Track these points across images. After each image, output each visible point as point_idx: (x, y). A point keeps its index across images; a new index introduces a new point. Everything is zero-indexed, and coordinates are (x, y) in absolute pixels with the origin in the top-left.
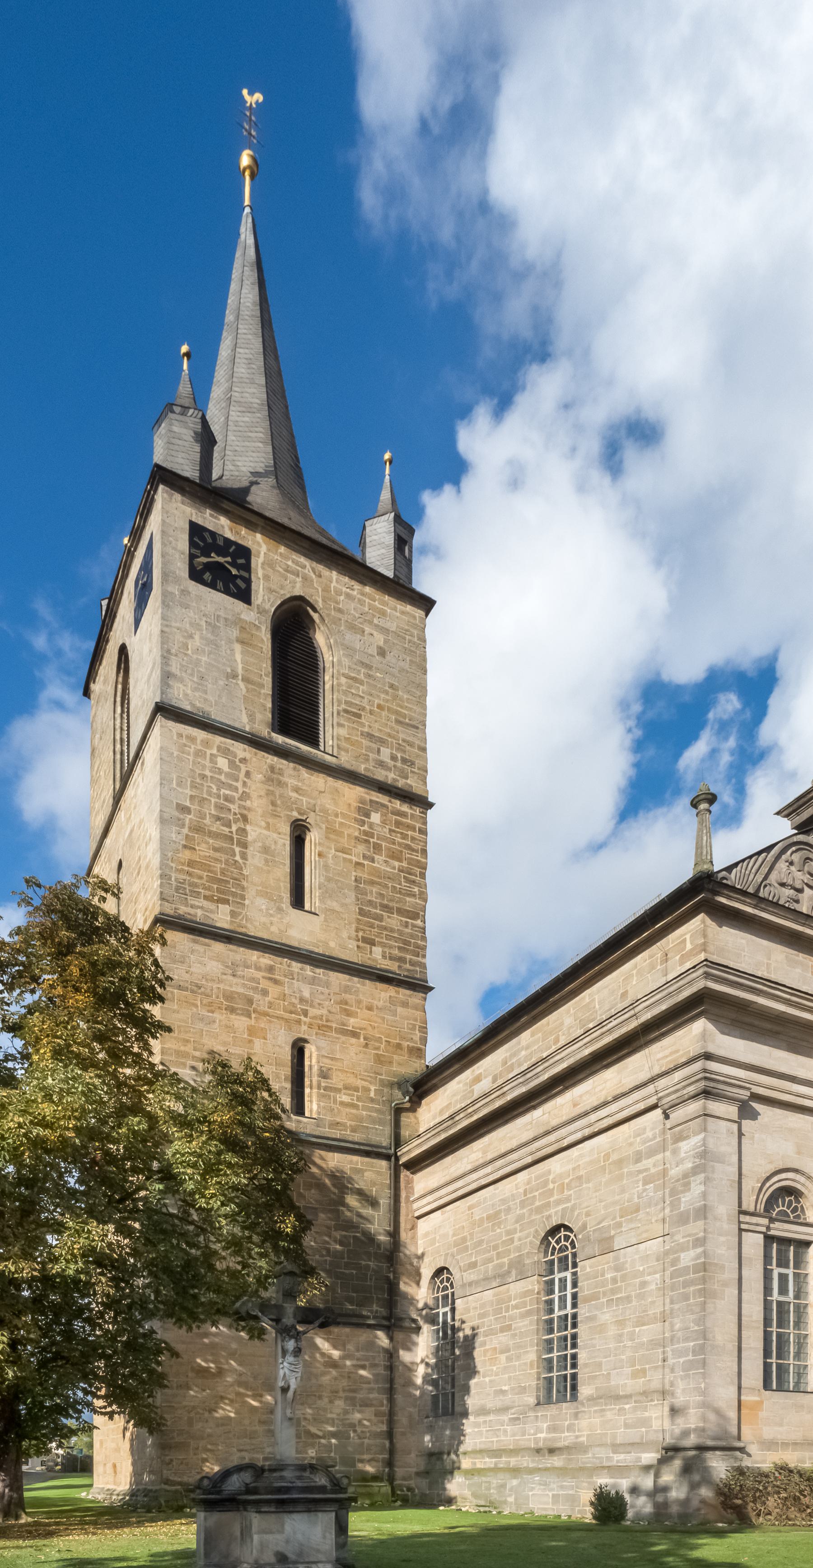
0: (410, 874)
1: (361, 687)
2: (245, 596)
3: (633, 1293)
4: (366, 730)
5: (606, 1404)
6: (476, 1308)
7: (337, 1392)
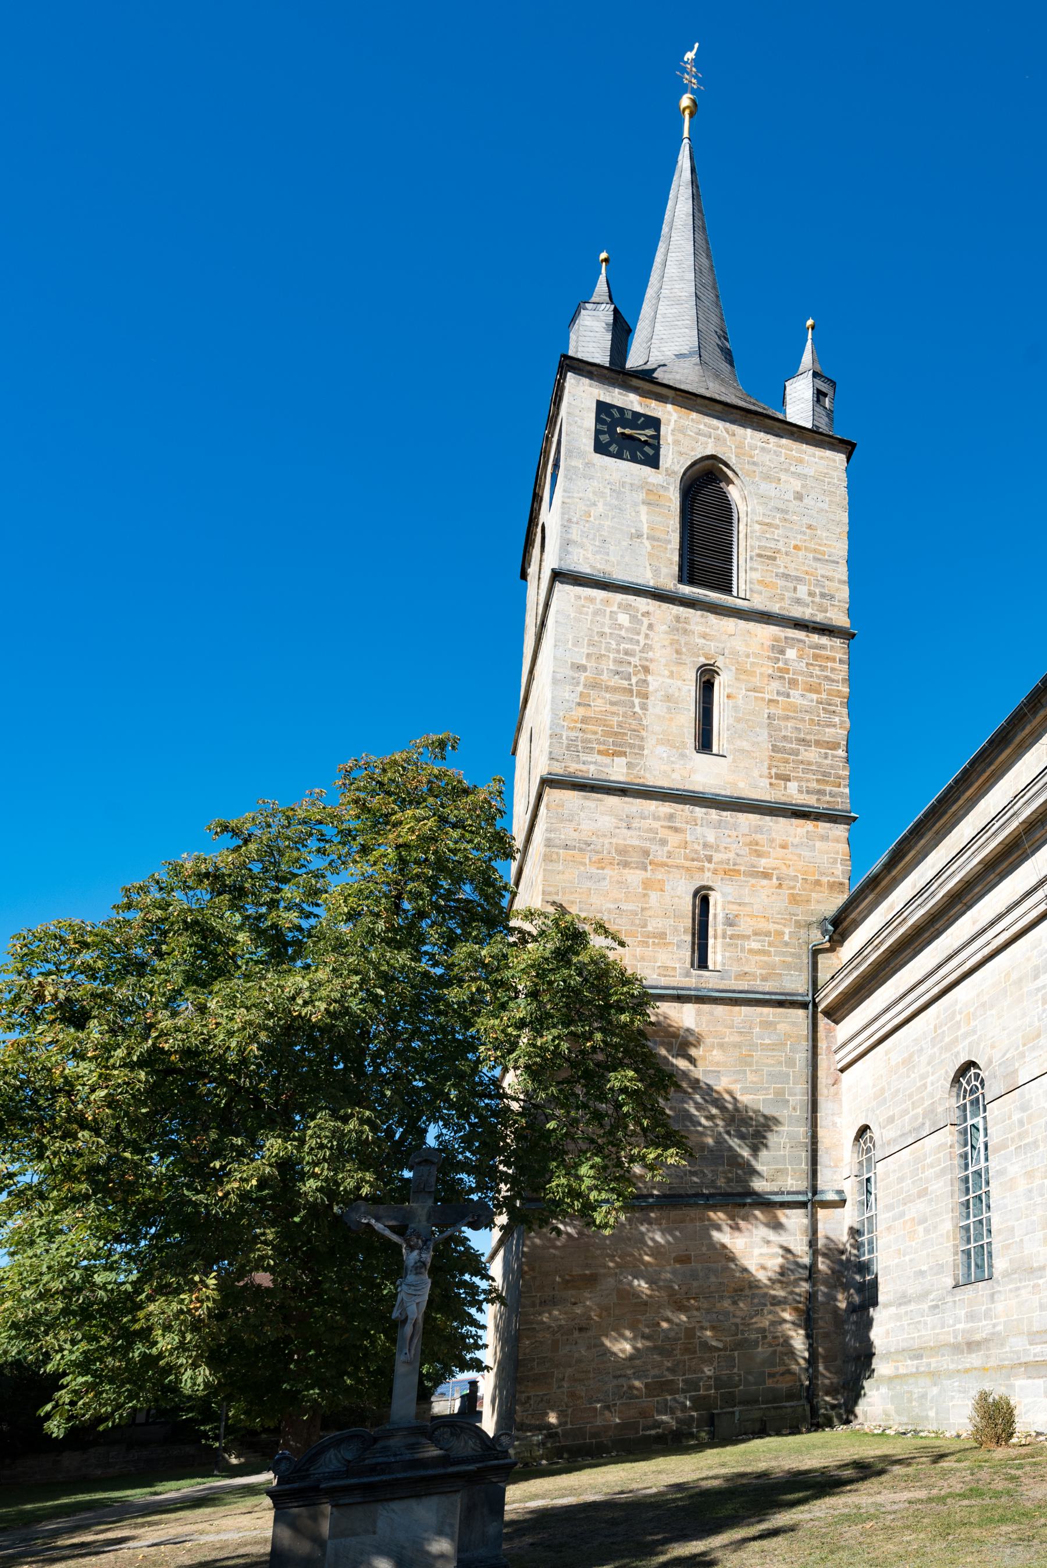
0: (830, 705)
1: (776, 531)
2: (653, 462)
3: (1040, 1137)
4: (781, 570)
5: (1020, 1280)
6: (895, 1171)
7: (741, 1290)
